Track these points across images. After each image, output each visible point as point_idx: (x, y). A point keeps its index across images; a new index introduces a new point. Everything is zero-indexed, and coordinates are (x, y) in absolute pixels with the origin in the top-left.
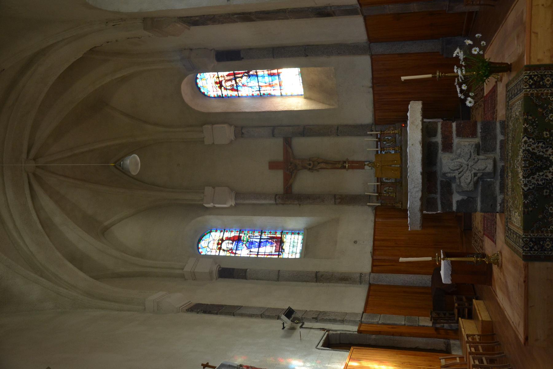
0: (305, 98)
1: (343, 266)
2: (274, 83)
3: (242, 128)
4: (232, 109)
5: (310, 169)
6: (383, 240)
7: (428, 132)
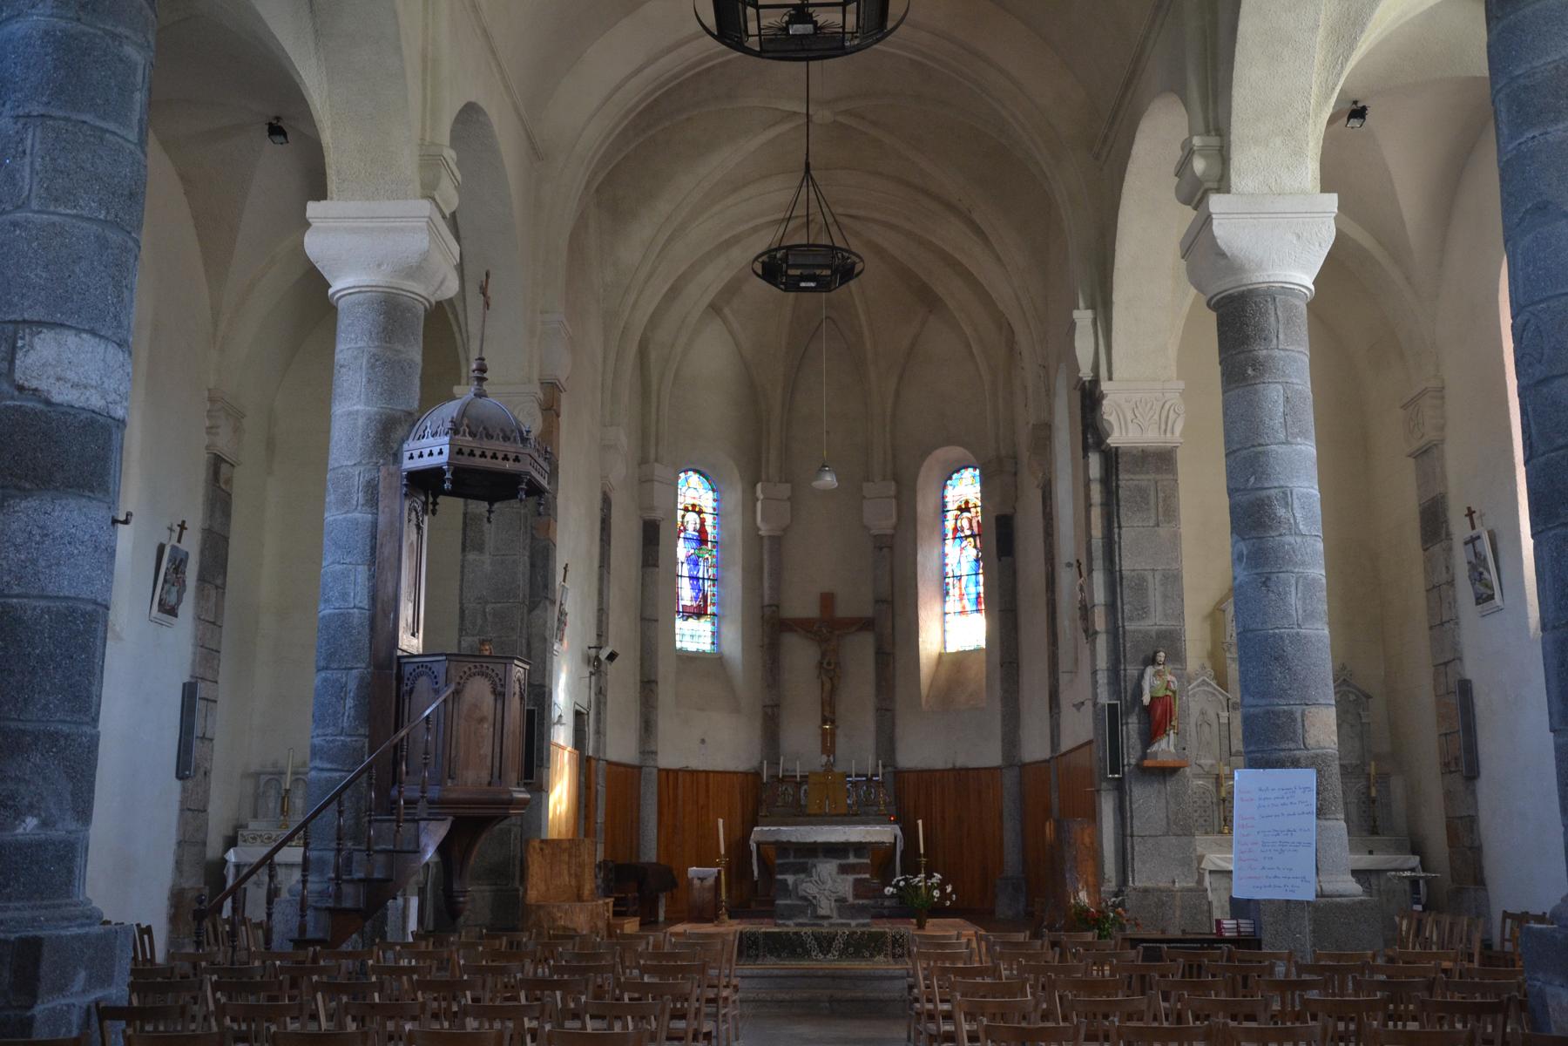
0: (940, 655)
1: (666, 724)
2: (965, 601)
3: (891, 548)
4: (922, 532)
5: (821, 663)
6: (707, 785)
7: (859, 848)
